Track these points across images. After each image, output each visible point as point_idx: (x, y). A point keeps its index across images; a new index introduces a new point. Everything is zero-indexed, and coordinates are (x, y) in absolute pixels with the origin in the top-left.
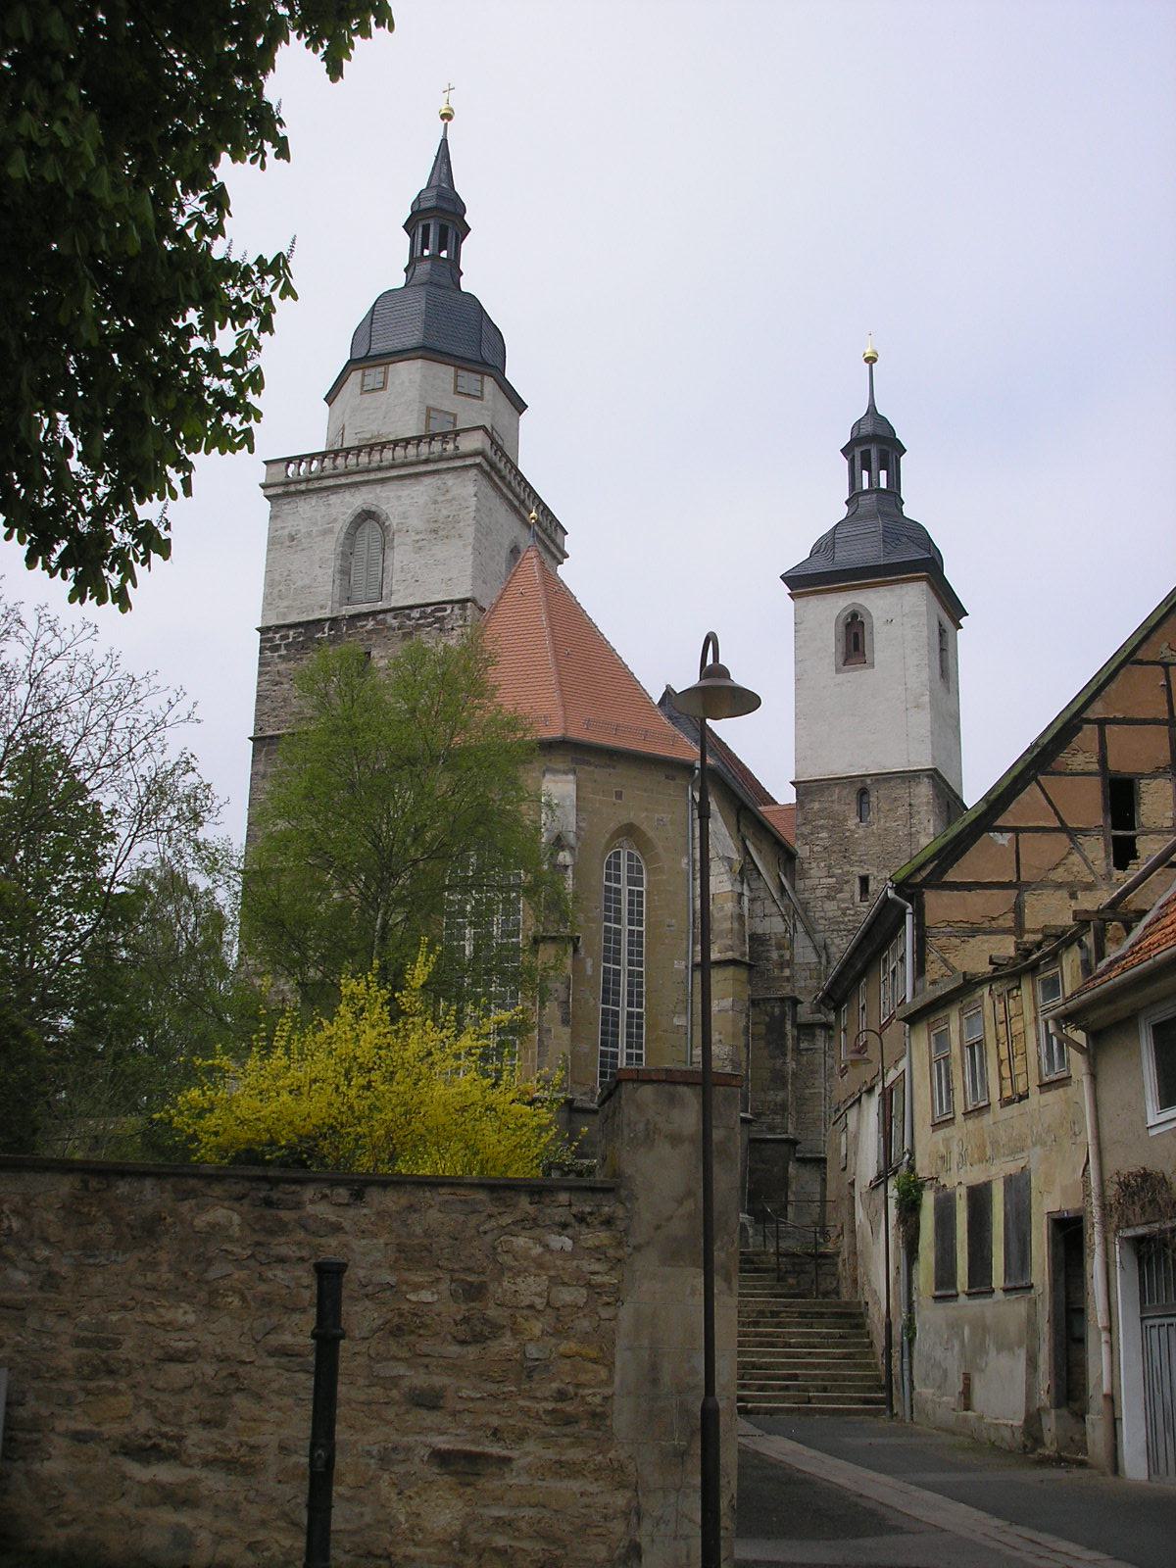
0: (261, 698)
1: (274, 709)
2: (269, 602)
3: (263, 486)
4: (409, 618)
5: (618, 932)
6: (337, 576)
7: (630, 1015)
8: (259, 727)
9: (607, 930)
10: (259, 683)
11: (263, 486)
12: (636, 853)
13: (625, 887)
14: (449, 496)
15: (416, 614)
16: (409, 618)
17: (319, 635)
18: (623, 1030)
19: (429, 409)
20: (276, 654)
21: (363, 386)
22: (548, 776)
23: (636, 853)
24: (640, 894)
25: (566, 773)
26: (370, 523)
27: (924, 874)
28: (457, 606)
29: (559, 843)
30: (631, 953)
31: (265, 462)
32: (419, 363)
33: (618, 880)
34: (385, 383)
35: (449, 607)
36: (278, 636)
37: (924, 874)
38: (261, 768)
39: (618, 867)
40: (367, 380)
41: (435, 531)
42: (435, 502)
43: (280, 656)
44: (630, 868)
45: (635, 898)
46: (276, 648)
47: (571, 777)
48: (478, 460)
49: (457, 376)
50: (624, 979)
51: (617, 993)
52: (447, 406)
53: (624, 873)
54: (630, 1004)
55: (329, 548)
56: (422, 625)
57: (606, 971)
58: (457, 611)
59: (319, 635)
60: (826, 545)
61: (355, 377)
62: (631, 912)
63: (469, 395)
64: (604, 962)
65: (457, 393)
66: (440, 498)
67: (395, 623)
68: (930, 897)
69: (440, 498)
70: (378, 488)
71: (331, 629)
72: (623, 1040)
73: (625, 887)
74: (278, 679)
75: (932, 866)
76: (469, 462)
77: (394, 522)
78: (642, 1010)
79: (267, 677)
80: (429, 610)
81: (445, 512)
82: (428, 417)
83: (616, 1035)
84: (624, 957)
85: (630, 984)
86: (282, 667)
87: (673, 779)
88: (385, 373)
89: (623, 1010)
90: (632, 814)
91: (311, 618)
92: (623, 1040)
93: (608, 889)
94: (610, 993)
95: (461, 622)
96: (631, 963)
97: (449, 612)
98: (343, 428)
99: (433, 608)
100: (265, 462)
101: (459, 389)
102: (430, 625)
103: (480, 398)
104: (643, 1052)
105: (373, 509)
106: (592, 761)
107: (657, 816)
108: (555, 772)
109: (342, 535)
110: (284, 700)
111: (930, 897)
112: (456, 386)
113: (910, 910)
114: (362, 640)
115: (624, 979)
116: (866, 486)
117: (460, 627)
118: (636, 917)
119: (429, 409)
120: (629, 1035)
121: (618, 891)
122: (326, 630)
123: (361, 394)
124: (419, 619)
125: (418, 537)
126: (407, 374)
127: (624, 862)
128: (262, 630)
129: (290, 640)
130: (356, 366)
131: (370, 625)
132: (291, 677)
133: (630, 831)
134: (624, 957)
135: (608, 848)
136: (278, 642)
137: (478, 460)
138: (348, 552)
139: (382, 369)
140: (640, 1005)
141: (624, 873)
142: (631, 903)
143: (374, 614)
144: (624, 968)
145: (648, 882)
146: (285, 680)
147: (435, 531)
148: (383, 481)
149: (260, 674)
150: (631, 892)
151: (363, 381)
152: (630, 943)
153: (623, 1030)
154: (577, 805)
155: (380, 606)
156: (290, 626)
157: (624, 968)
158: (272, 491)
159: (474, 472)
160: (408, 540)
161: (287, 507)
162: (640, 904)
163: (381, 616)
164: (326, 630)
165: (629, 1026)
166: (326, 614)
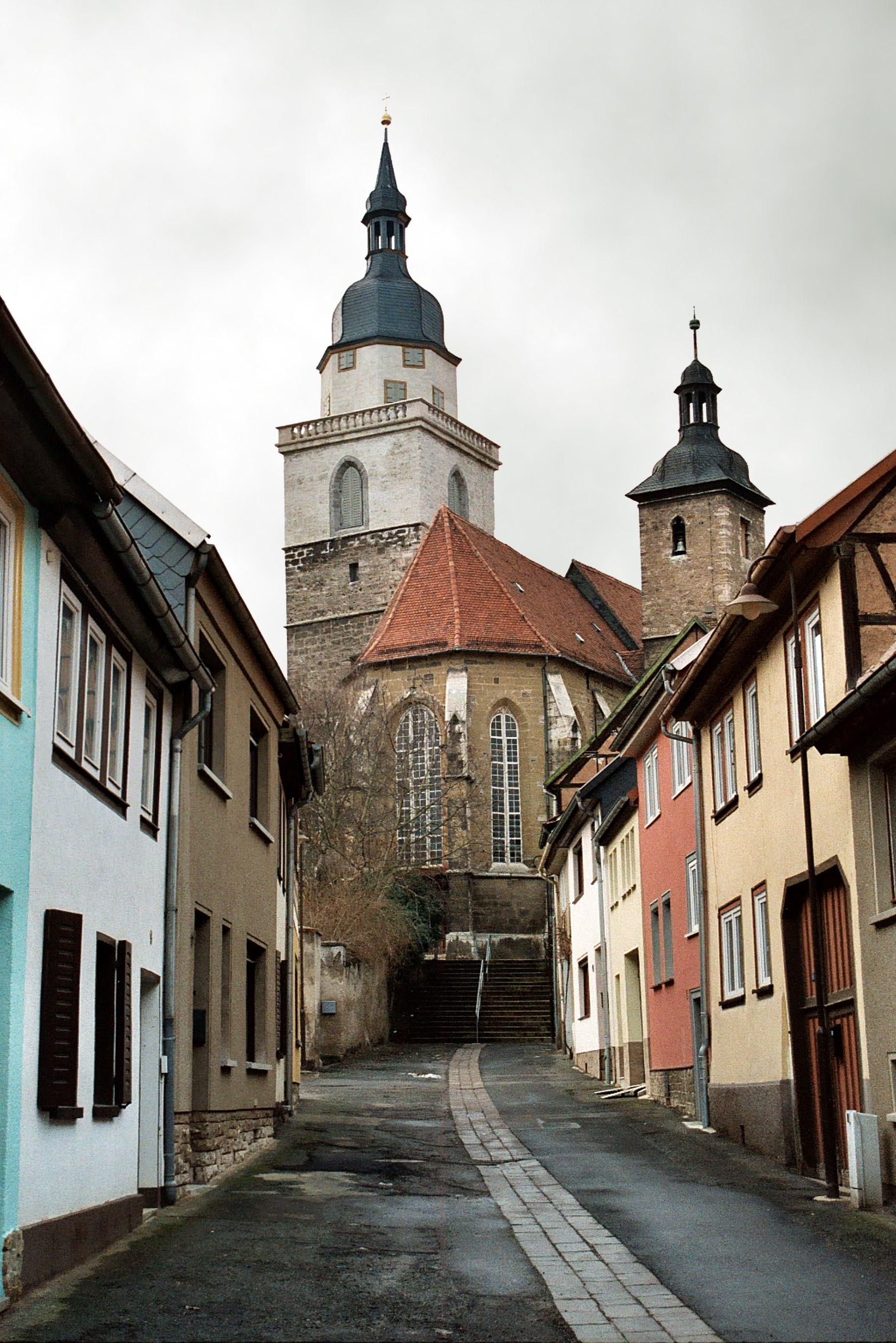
0: (289, 598)
1: (298, 606)
2: (289, 528)
3: (278, 446)
4: (382, 538)
5: (501, 767)
6: (333, 509)
7: (511, 817)
8: (290, 620)
9: (494, 766)
10: (287, 587)
11: (278, 446)
12: (511, 716)
13: (504, 738)
14: (401, 449)
15: (385, 535)
16: (382, 538)
17: (324, 552)
18: (507, 826)
19: (386, 382)
20: (296, 566)
21: (339, 366)
22: (450, 674)
23: (511, 716)
24: (515, 741)
25: (461, 671)
26: (351, 469)
27: (561, 780)
28: (412, 529)
29: (455, 720)
30: (510, 779)
31: (278, 428)
32: (377, 347)
33: (499, 734)
34: (354, 363)
35: (407, 529)
36: (296, 553)
37: (561, 780)
38: (293, 647)
39: (499, 726)
40: (343, 361)
41: (395, 475)
42: (393, 454)
43: (299, 568)
44: (508, 726)
45: (512, 744)
46: (295, 562)
47: (464, 673)
48: (418, 423)
49: (404, 353)
50: (506, 795)
51: (502, 804)
52: (399, 378)
53: (503, 730)
54: (511, 810)
55: (324, 489)
56: (390, 543)
57: (495, 791)
58: (412, 533)
59: (324, 552)
60: (664, 467)
61: (334, 358)
62: (509, 754)
63: (413, 366)
64: (493, 785)
65: (405, 366)
66: (396, 451)
67: (372, 541)
68: (564, 791)
69: (396, 451)
70: (354, 444)
71: (331, 548)
72: (507, 832)
73: (504, 738)
74: (299, 584)
75: (564, 777)
76: (412, 424)
77: (367, 468)
78: (519, 813)
79: (292, 583)
80: (394, 532)
81: (400, 461)
82: (386, 388)
83: (503, 829)
84: (506, 781)
85: (511, 798)
86: (301, 575)
87: (533, 665)
88: (354, 355)
89: (507, 814)
90: (506, 691)
91: (317, 540)
92: (507, 832)
93: (493, 740)
94: (498, 804)
95: (415, 540)
96: (510, 785)
97: (407, 532)
98: (329, 397)
99: (396, 530)
100: (278, 428)
101: (407, 363)
102: (395, 543)
103: (423, 367)
104: (521, 838)
105: (352, 460)
106: (478, 660)
107: (522, 691)
108: (455, 670)
109: (333, 479)
110: (304, 599)
111: (564, 791)
112: (404, 361)
113: (555, 798)
114: (352, 555)
115: (506, 795)
116: (692, 421)
117: (415, 543)
118: (513, 756)
119: (386, 382)
120: (511, 829)
121: (500, 741)
122: (328, 548)
123: (339, 372)
124: (388, 539)
125: (383, 480)
126: (368, 355)
127: (503, 722)
128: (287, 550)
129: (305, 556)
130: (334, 351)
131: (356, 543)
132: (308, 582)
133: (505, 702)
134: (506, 781)
135: (491, 714)
136: (297, 558)
137: (418, 423)
138: (337, 492)
139: (351, 352)
140: (517, 810)
141: (503, 730)
142: (509, 748)
143: (358, 536)
144: (506, 787)
145: (520, 733)
146: (304, 585)
147: (395, 475)
148: (358, 439)
149: (287, 580)
150: (509, 741)
151: (339, 362)
152: (509, 773)
153: (507, 826)
154: (468, 691)
155: (362, 530)
156: (304, 546)
157: (506, 787)
158: (285, 449)
159: (417, 431)
160: (378, 482)
161: (294, 459)
162: (515, 747)
163: (363, 537)
164: (328, 548)
165: (511, 823)
166: (327, 537)
